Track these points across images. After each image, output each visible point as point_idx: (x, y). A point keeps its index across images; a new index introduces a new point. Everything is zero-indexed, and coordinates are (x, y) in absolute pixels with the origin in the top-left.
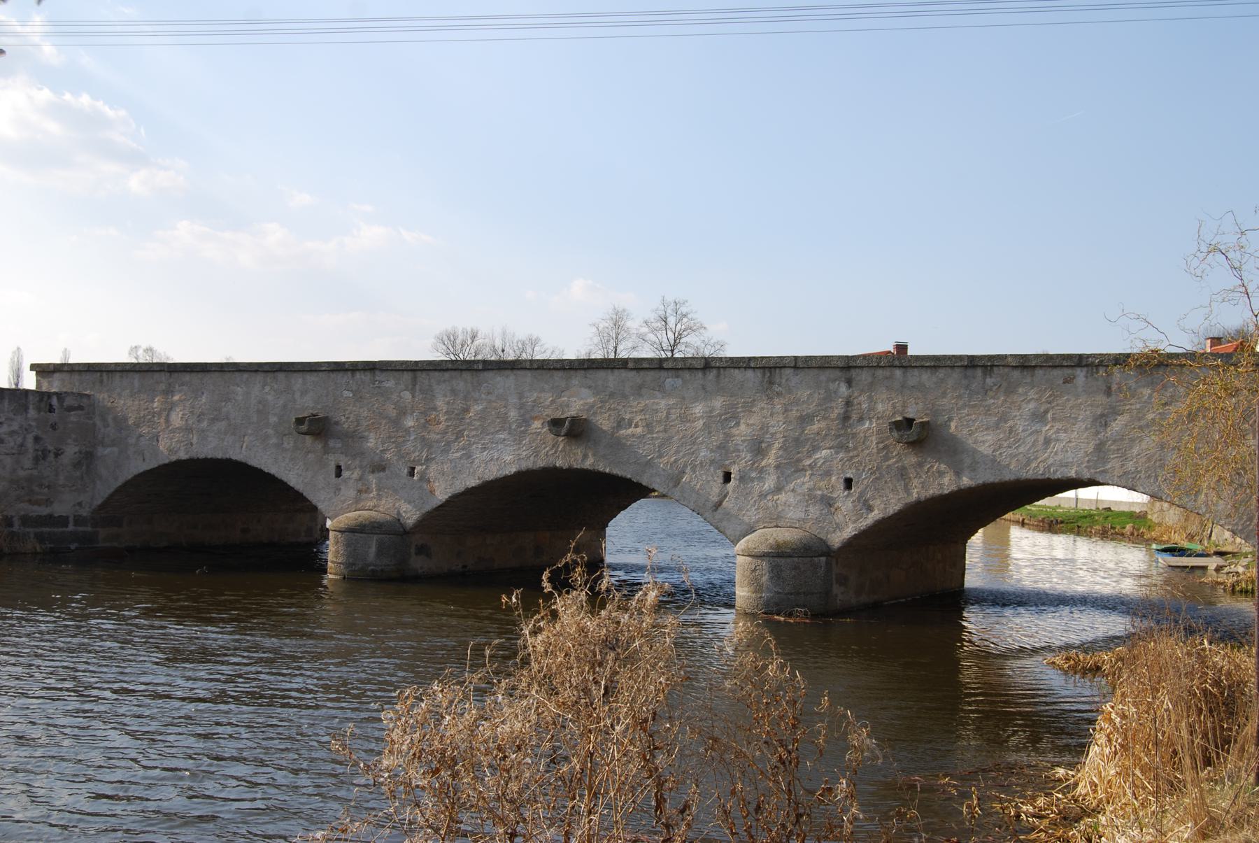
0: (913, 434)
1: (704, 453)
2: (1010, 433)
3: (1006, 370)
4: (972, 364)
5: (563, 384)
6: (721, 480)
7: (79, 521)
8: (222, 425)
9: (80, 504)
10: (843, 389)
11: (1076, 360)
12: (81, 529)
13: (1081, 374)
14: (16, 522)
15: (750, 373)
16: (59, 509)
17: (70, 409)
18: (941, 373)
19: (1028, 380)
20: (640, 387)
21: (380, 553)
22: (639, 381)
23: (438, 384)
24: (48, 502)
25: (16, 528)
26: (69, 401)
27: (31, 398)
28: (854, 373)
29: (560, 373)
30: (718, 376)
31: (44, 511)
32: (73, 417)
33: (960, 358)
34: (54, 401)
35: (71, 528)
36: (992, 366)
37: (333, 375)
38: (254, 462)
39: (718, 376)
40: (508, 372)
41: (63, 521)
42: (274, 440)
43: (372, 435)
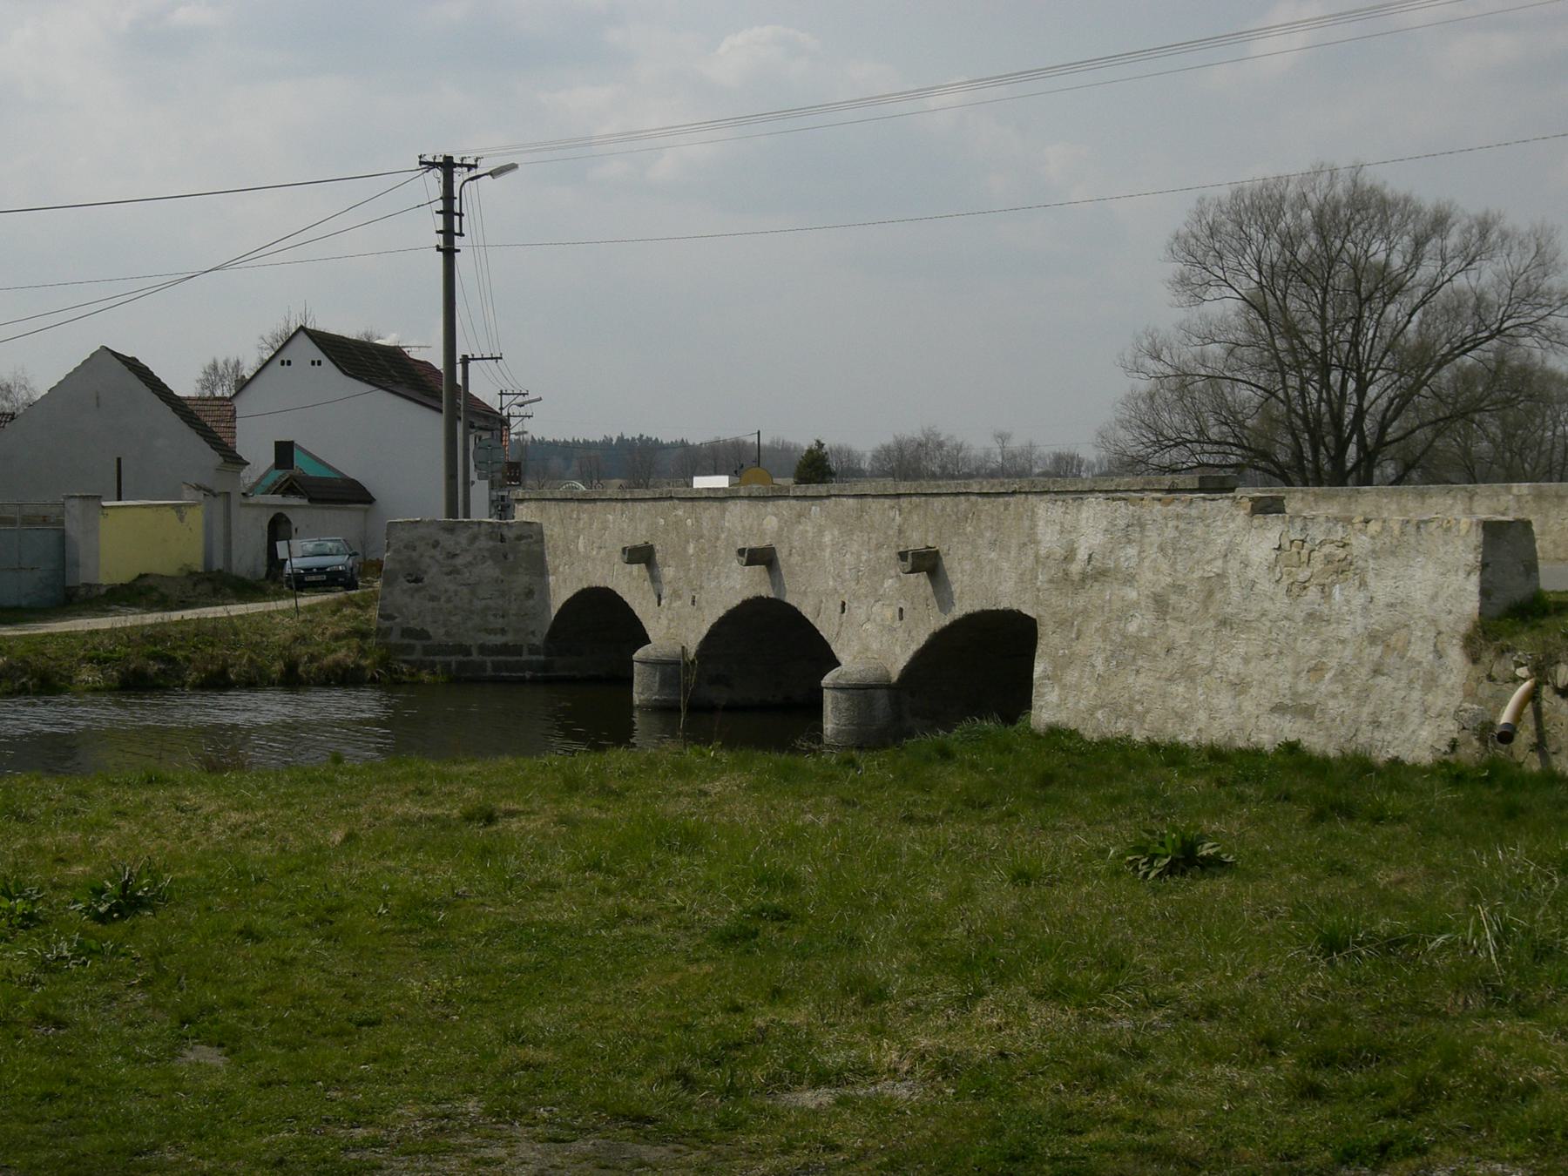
7: (533, 650)
12: (534, 658)
14: (475, 651)
35: (525, 657)
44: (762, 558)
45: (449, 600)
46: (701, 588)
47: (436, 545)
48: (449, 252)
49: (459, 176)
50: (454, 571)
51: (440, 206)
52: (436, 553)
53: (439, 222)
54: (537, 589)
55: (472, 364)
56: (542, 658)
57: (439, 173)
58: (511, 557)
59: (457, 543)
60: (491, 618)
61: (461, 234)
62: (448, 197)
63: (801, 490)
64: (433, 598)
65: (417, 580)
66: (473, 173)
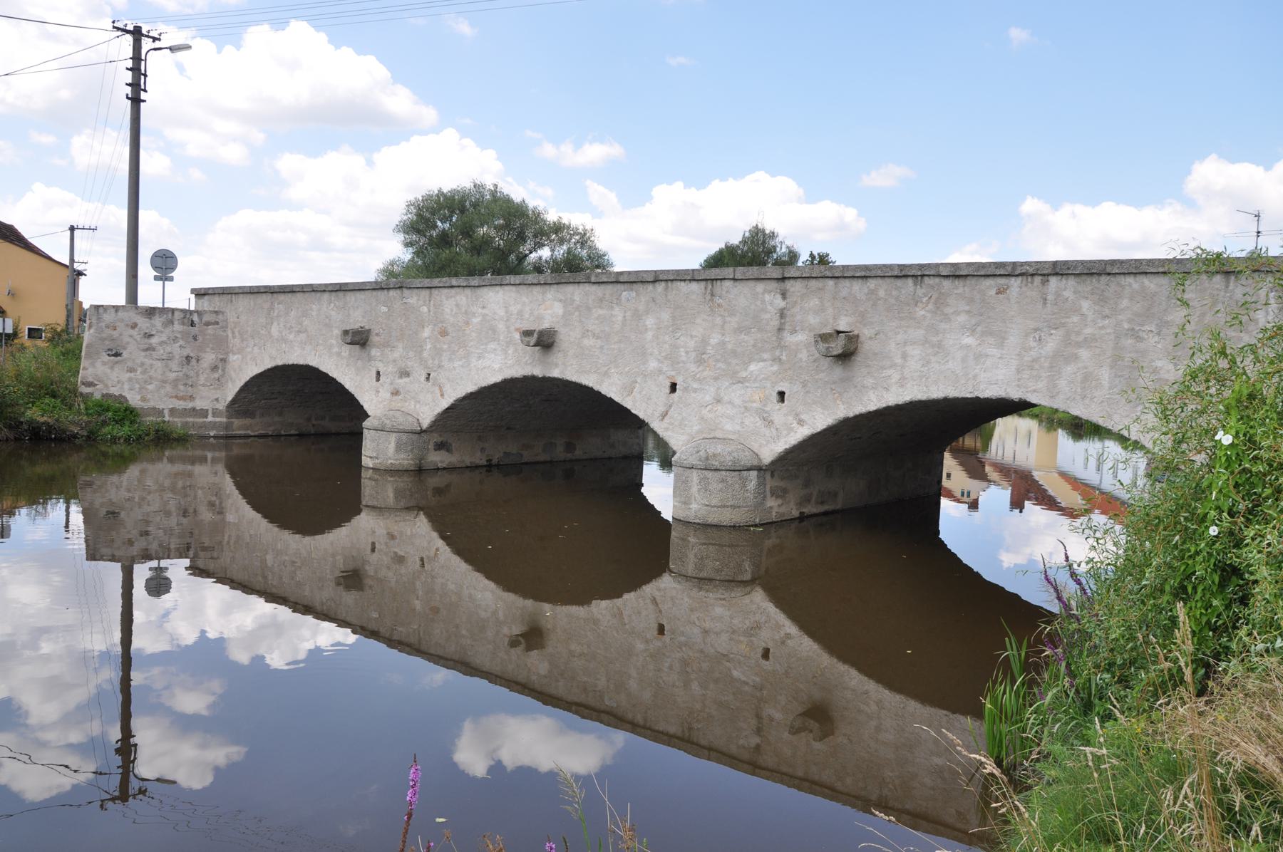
0: (838, 346)
1: (653, 364)
2: (147, 350)
3: (937, 280)
4: (902, 273)
5: (540, 298)
6: (668, 390)
7: (216, 413)
8: (303, 336)
9: (217, 400)
10: (780, 303)
11: (1009, 269)
12: (218, 420)
13: (1015, 283)
14: (166, 412)
15: (694, 286)
16: (199, 404)
17: (208, 324)
18: (872, 283)
19: (960, 291)
20: (601, 300)
21: (399, 448)
22: (600, 294)
23: (447, 298)
24: (192, 398)
25: (167, 418)
26: (206, 318)
27: (176, 313)
28: (788, 284)
29: (538, 288)
30: (667, 288)
31: (190, 405)
32: (210, 330)
33: (890, 267)
34: (195, 318)
35: (210, 419)
36: (923, 276)
37: (375, 293)
38: (323, 369)
39: (667, 288)
40: (498, 288)
41: (204, 413)
42: (335, 350)
43: (400, 345)
44: (545, 342)
45: (144, 372)
46: (440, 366)
47: (134, 326)
48: (136, 101)
49: (146, 44)
50: (150, 349)
51: (130, 64)
52: (134, 332)
53: (128, 77)
54: (953, 452)
55: (76, 232)
56: (224, 420)
57: (129, 39)
58: (200, 338)
59: (153, 326)
60: (182, 387)
61: (145, 91)
62: (137, 58)
63: (427, 282)
64: (131, 370)
65: (117, 355)
66: (157, 44)
